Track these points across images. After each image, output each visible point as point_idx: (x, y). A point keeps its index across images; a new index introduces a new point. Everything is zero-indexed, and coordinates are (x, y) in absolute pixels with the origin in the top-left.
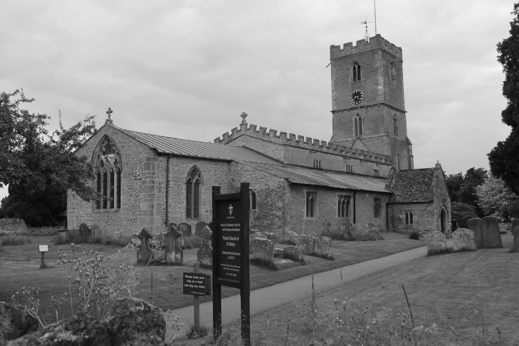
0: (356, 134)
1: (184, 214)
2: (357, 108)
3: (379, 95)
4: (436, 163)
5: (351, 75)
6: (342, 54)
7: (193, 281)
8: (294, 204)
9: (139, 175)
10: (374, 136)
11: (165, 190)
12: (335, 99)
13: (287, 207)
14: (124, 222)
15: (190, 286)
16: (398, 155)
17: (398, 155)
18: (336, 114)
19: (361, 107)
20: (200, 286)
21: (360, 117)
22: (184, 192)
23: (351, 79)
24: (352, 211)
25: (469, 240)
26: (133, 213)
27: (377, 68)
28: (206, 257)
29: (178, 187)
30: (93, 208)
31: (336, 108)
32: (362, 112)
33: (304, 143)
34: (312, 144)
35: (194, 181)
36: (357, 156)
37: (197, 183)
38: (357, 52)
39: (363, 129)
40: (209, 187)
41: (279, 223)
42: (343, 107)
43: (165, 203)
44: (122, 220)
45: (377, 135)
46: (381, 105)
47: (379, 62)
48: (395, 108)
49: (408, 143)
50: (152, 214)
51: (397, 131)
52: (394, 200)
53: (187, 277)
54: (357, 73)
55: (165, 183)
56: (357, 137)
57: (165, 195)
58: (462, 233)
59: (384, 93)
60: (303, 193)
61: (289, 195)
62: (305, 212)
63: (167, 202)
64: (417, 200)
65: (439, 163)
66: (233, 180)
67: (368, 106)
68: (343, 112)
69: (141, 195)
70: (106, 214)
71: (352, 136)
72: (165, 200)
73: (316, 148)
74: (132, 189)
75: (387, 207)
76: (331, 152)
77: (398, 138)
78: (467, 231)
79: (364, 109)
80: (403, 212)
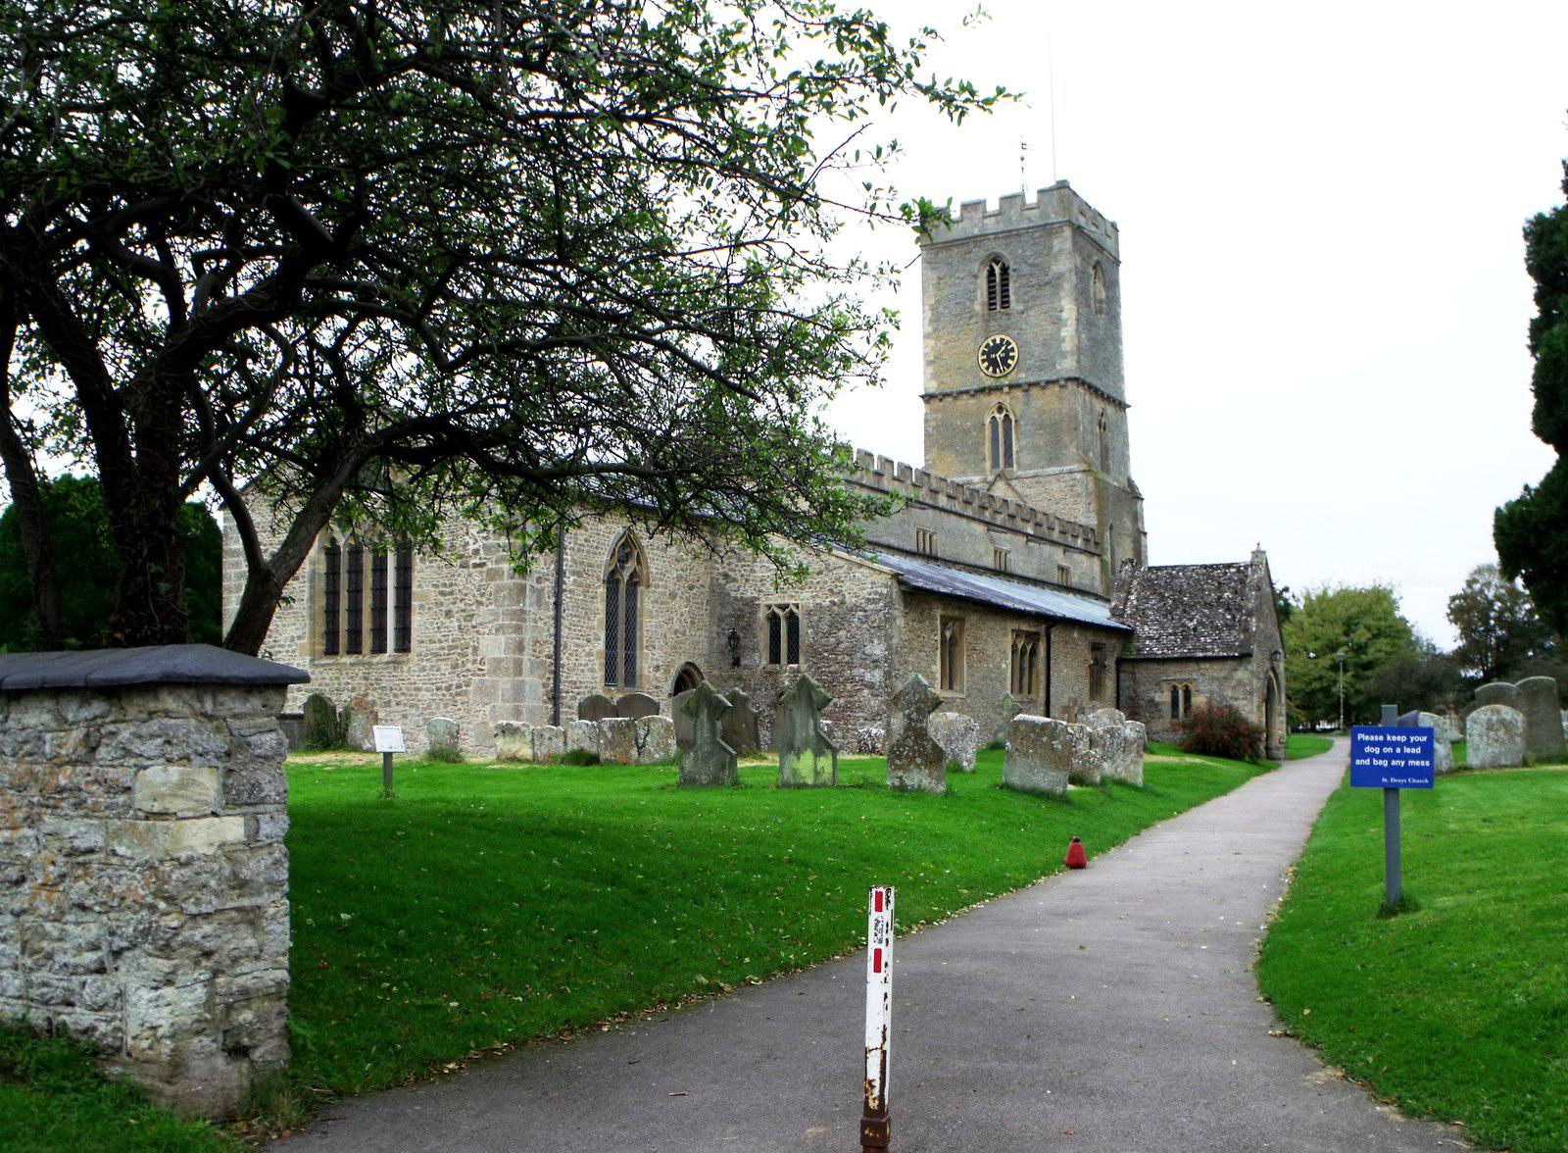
0: (995, 464)
1: (600, 674)
2: (999, 389)
3: (1064, 355)
4: (1254, 549)
5: (982, 294)
6: (956, 232)
7: (1387, 750)
8: (912, 650)
9: (476, 552)
10: (1049, 470)
11: (552, 600)
12: (933, 361)
13: (896, 658)
14: (425, 696)
15: (1375, 762)
16: (1111, 528)
17: (1111, 528)
18: (936, 403)
19: (1012, 387)
20: (1411, 762)
21: (1006, 416)
22: (600, 606)
23: (983, 305)
24: (1043, 677)
25: (1512, 738)
26: (455, 667)
27: (1060, 276)
28: (918, 766)
29: (585, 593)
30: (313, 653)
31: (933, 388)
32: (1013, 401)
33: (894, 479)
34: (914, 485)
35: (626, 575)
36: (1019, 524)
37: (634, 584)
38: (1001, 227)
39: (1015, 448)
40: (664, 594)
41: (875, 703)
42: (954, 384)
43: (552, 639)
44: (418, 689)
45: (1056, 470)
46: (1069, 384)
47: (1064, 259)
48: (1102, 394)
49: (1133, 495)
50: (518, 668)
51: (1107, 458)
52: (1139, 650)
53: (1367, 738)
54: (998, 289)
55: (552, 579)
56: (998, 471)
57: (552, 613)
58: (1495, 718)
59: (1079, 348)
60: (933, 618)
61: (900, 622)
62: (938, 676)
63: (557, 636)
64: (1207, 650)
65: (1262, 548)
66: (726, 576)
67: (1030, 385)
68: (955, 398)
69: (483, 614)
70: (360, 671)
71: (983, 471)
72: (552, 631)
73: (923, 495)
74: (451, 593)
75: (1118, 671)
76: (958, 508)
77: (1109, 479)
78: (1507, 712)
79: (1018, 393)
80: (1164, 685)
